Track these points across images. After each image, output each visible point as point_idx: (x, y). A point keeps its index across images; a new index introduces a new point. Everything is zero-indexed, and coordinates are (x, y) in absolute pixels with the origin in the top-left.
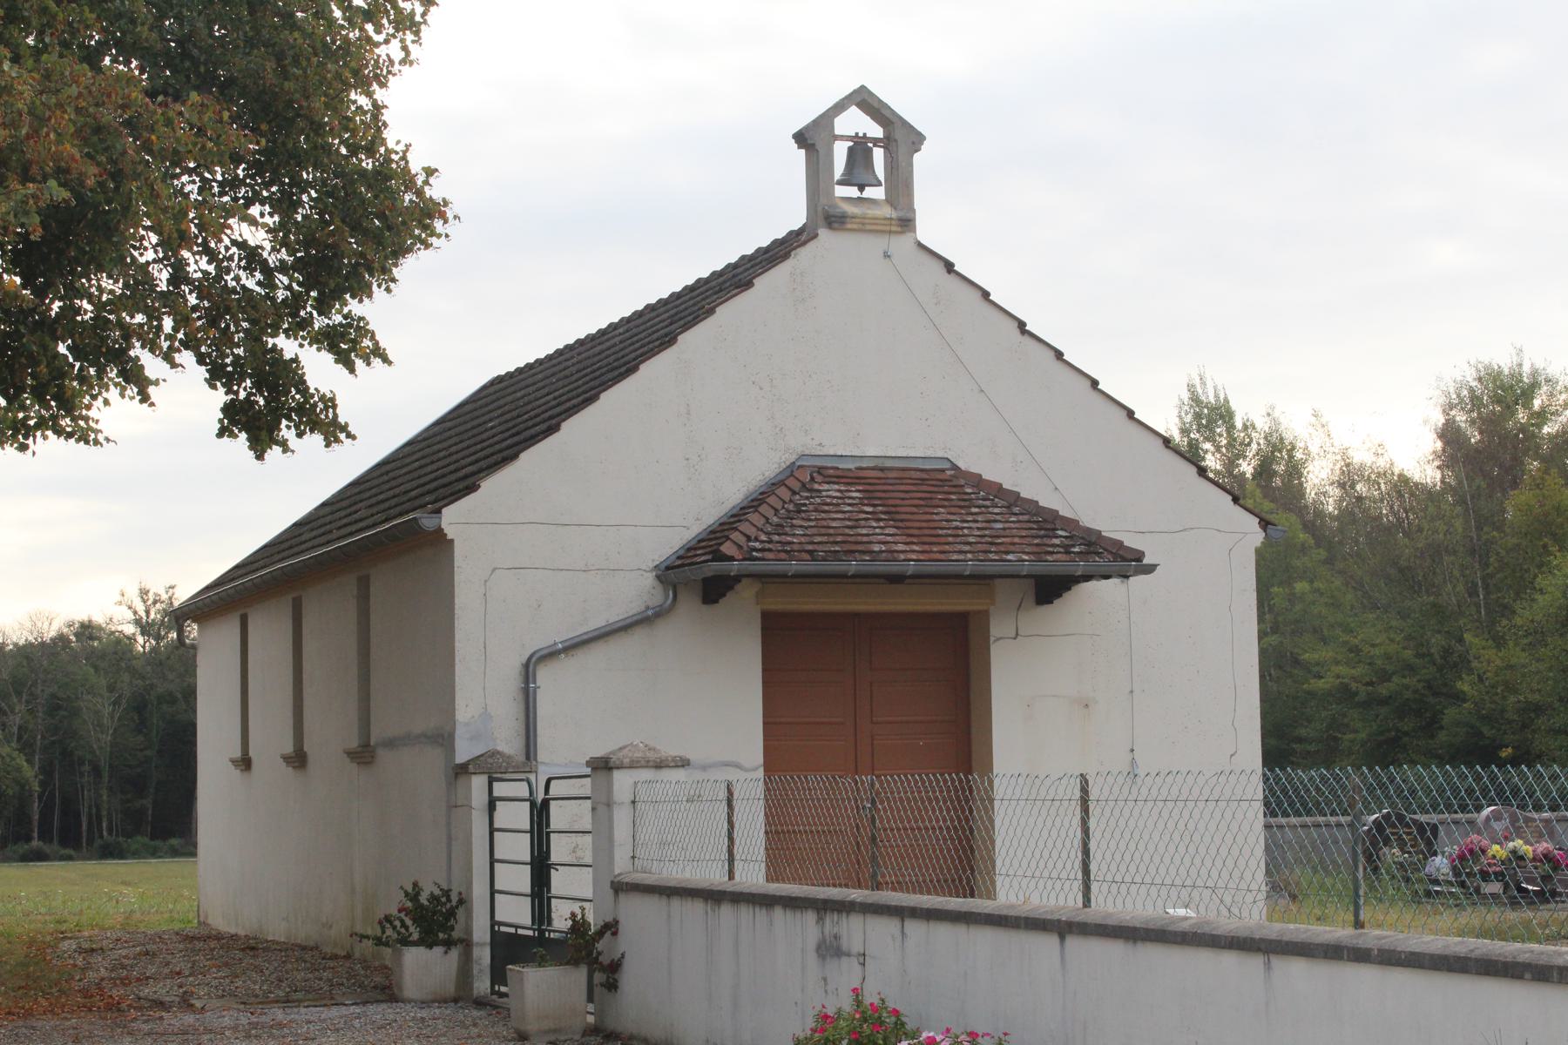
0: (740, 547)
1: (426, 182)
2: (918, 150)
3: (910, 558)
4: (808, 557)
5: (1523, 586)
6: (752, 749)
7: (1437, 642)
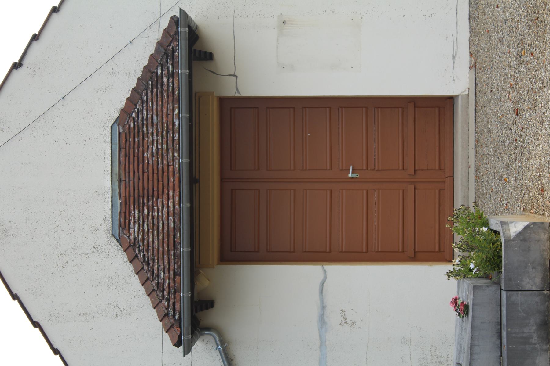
4: (178, 278)
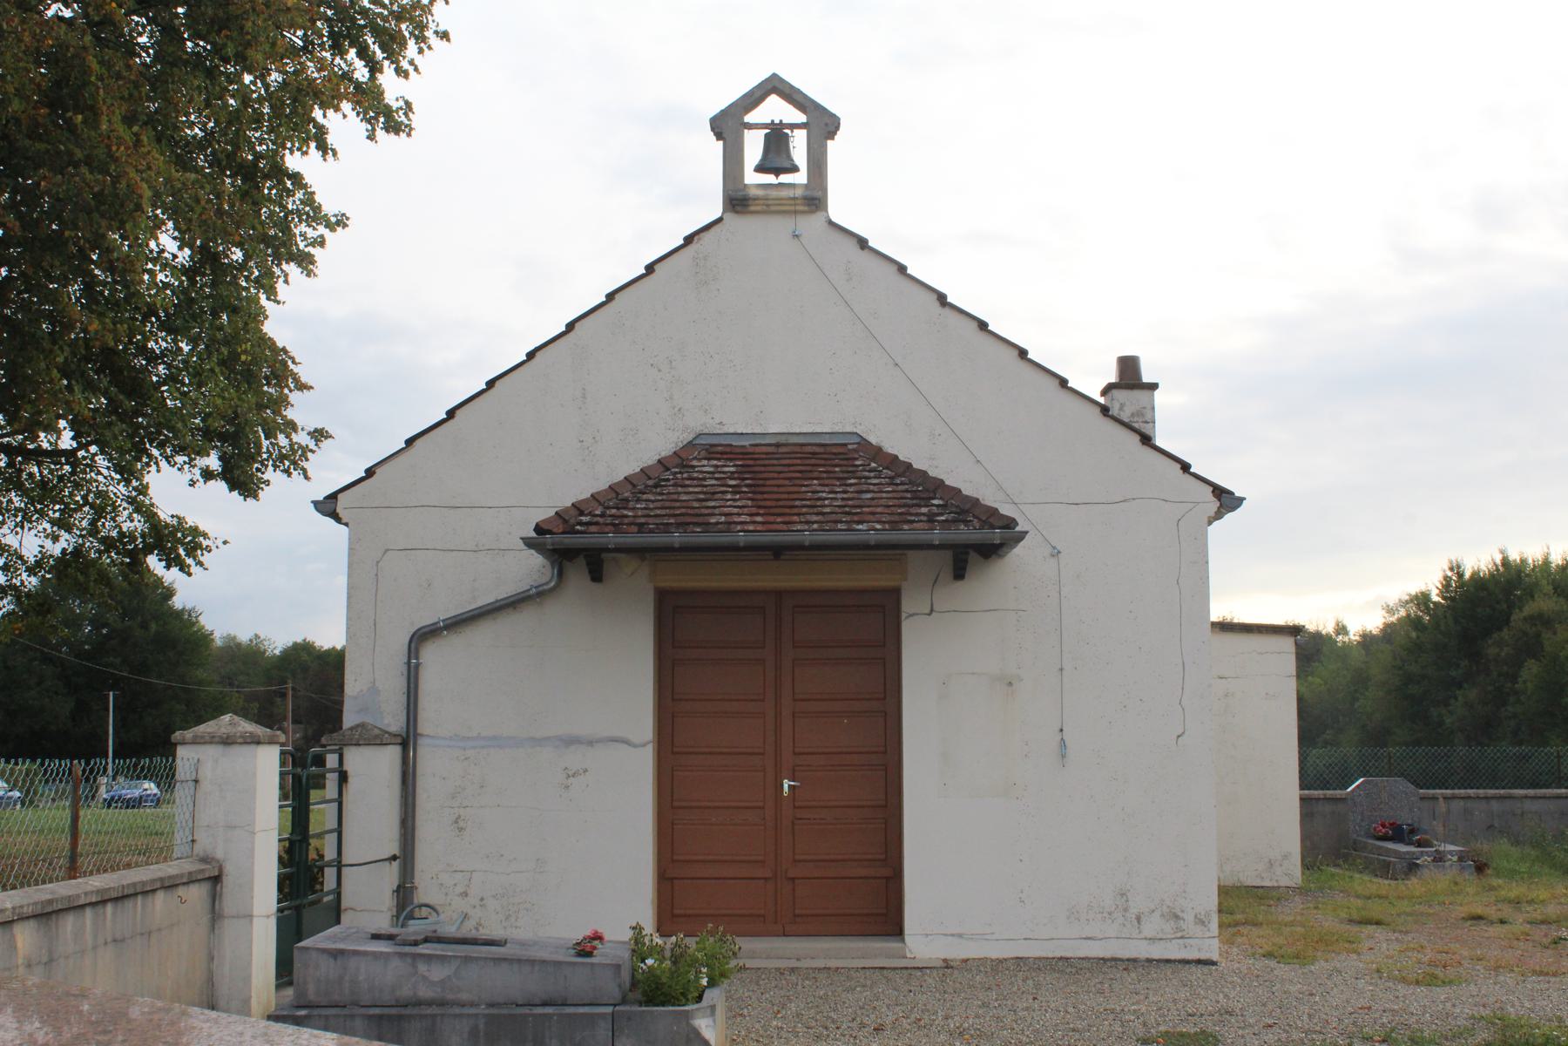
4: (635, 529)
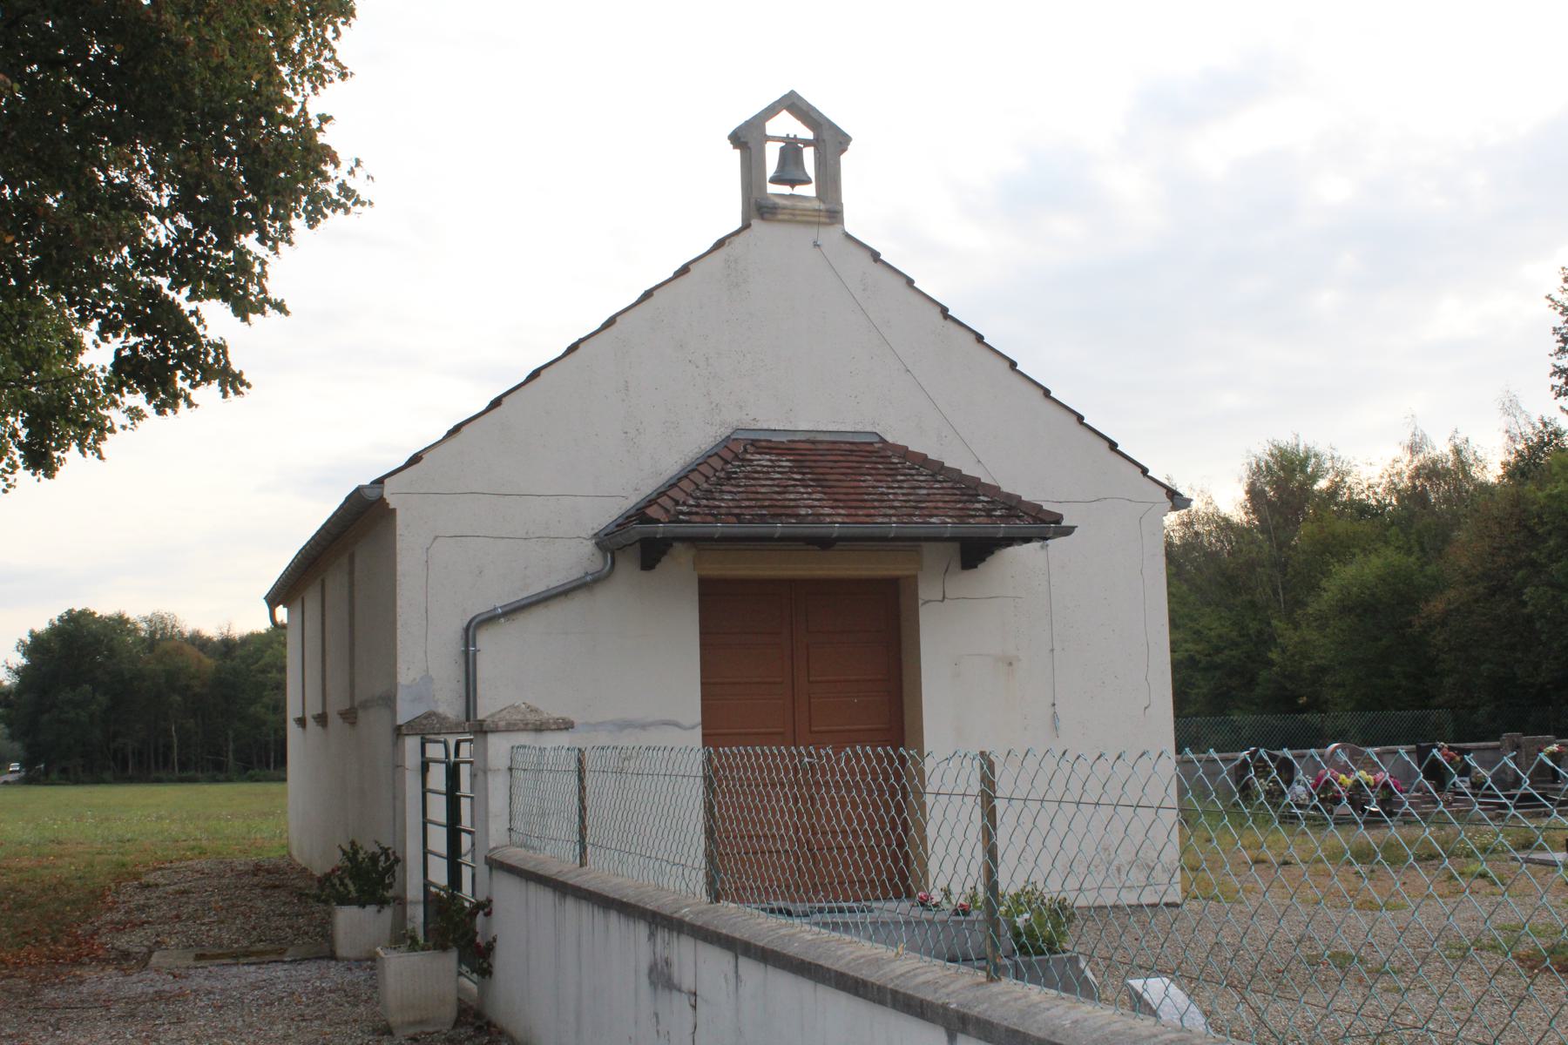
0: (667, 511)
1: (320, 129)
2: (844, 150)
3: (836, 523)
5: (1314, 588)
6: (690, 707)
7: (1253, 626)
